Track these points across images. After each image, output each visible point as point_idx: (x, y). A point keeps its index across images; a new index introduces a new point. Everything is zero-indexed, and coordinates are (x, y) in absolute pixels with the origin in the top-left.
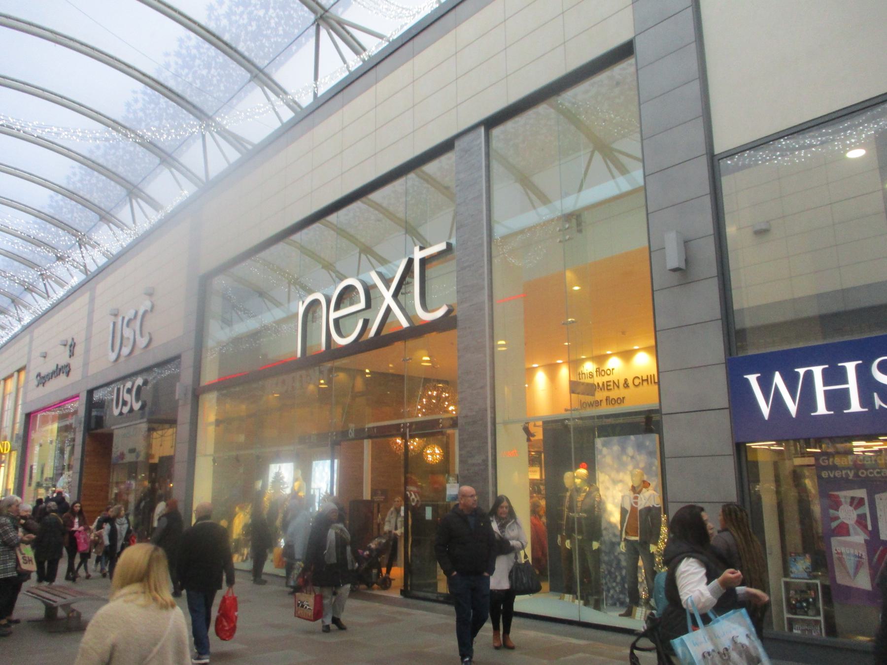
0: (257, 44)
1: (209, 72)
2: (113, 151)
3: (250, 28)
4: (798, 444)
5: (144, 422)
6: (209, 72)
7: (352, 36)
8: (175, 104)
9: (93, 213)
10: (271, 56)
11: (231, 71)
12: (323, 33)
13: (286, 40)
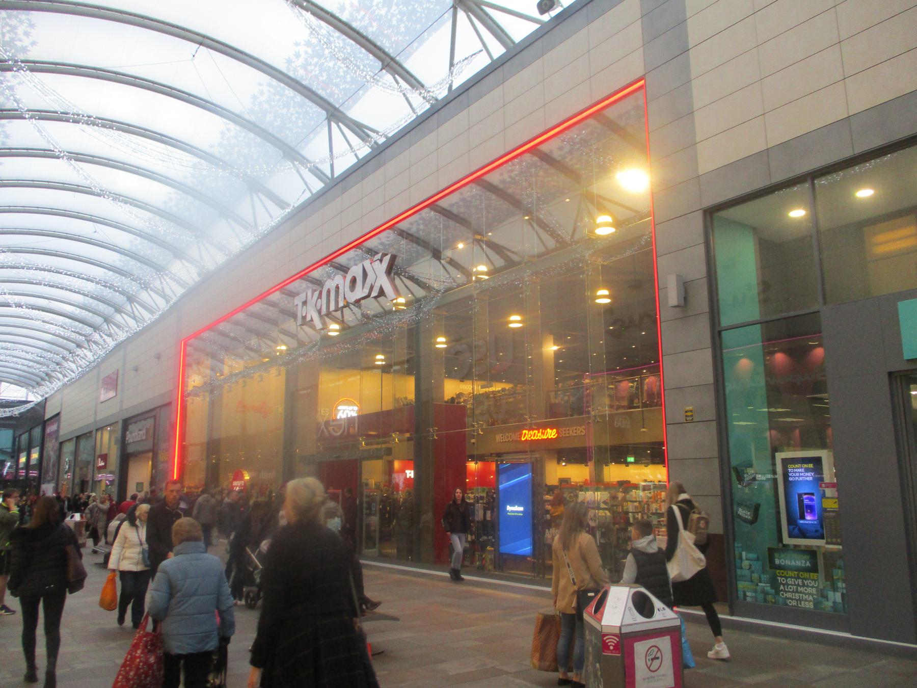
0: (409, 8)
1: (388, 11)
3: (321, 78)
7: (491, 18)
8: (353, 43)
9: (100, 318)
10: (341, 101)
11: (308, 109)
12: (333, 125)
13: (407, 38)
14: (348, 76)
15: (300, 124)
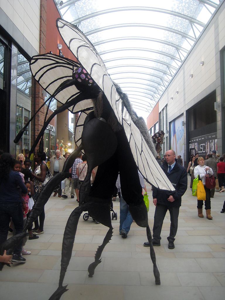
2: (181, 4)
3: (186, 6)
4: (168, 214)
5: (215, 149)
14: (195, 4)
15: (195, 5)
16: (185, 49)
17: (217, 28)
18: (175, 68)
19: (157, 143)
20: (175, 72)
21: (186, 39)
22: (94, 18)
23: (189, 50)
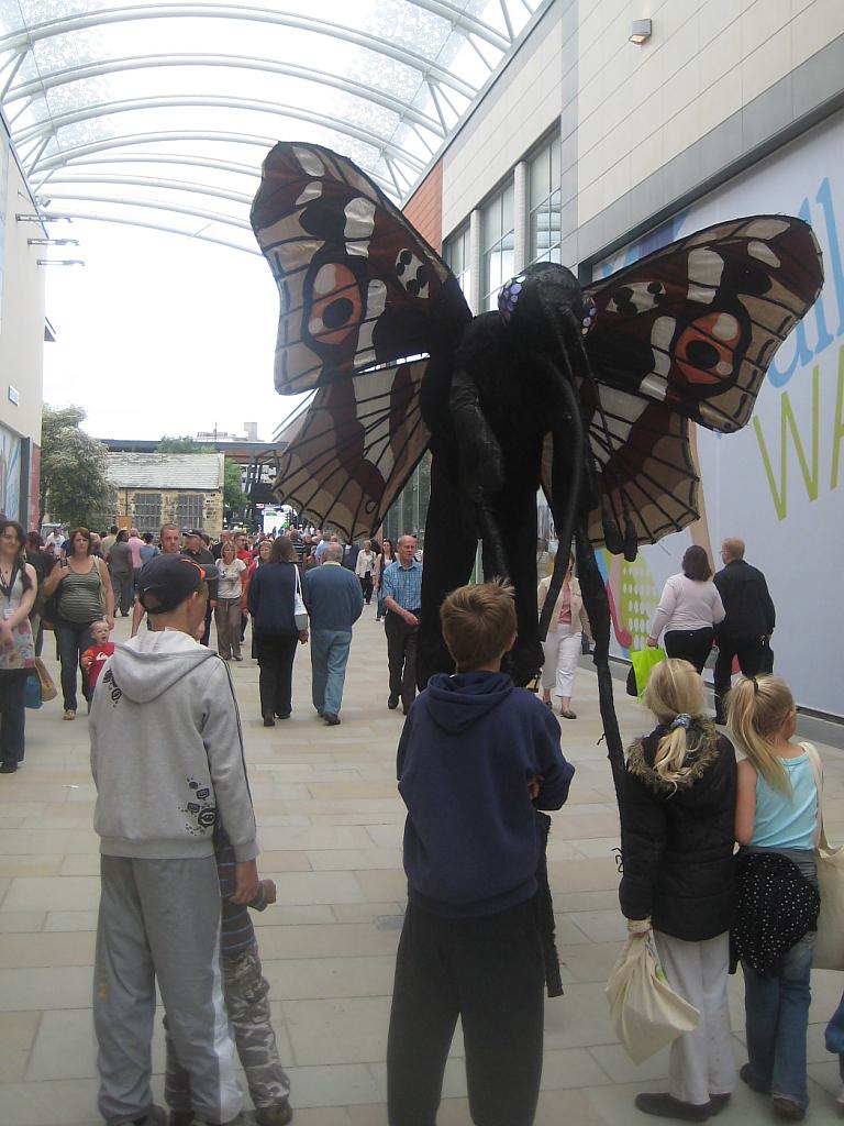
6: (418, 21)
14: (436, 33)
16: (463, 82)
17: (570, 37)
18: (408, 156)
19: (654, 387)
20: (464, 106)
21: (469, 39)
22: (84, 33)
23: (479, 88)
